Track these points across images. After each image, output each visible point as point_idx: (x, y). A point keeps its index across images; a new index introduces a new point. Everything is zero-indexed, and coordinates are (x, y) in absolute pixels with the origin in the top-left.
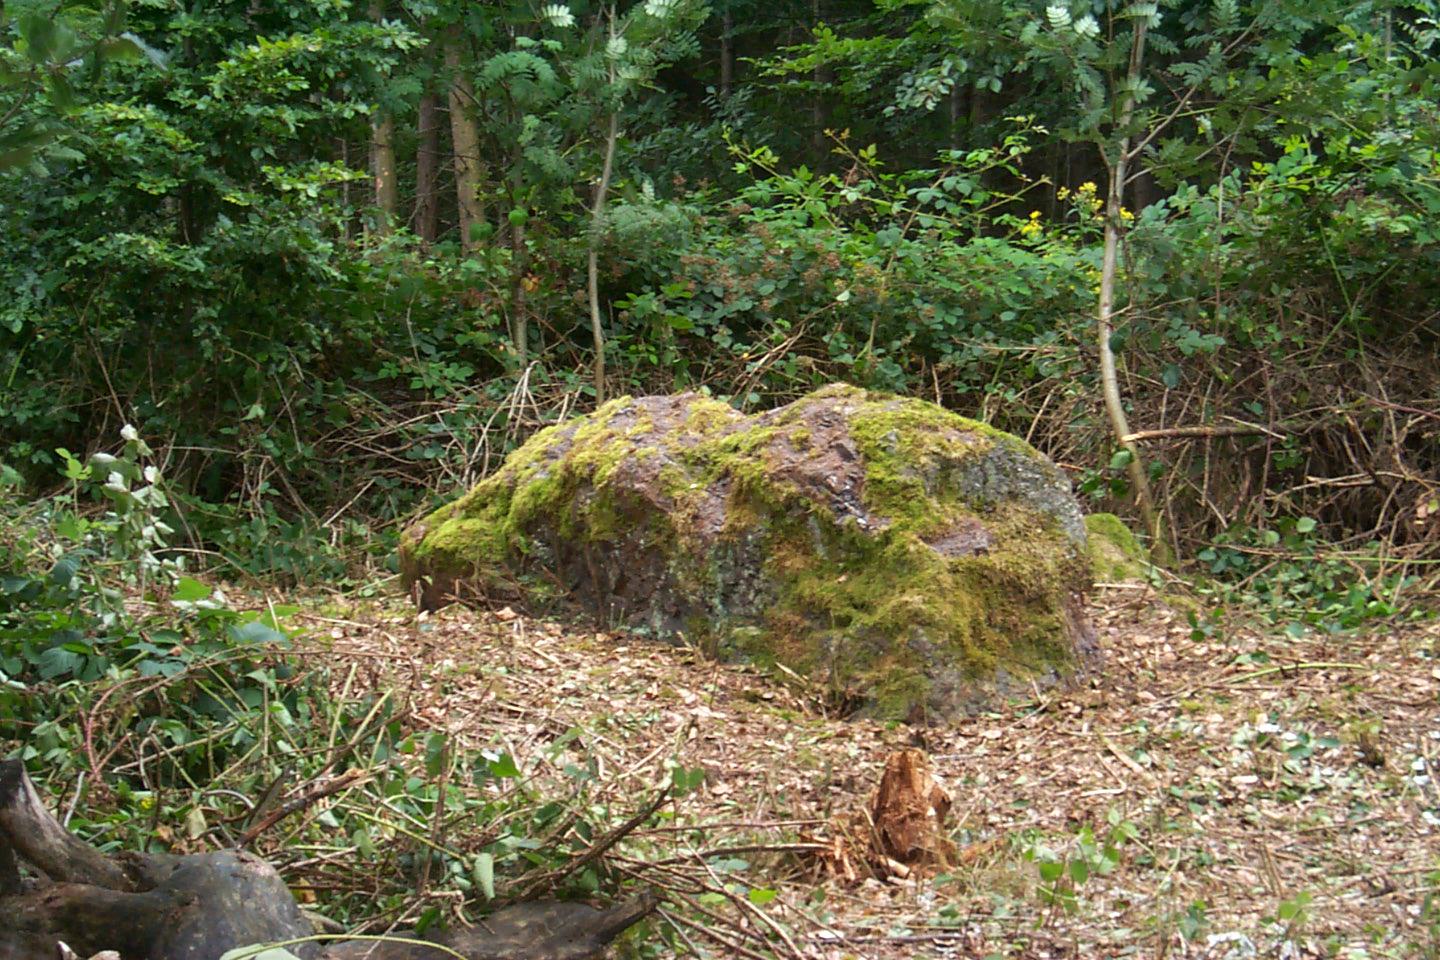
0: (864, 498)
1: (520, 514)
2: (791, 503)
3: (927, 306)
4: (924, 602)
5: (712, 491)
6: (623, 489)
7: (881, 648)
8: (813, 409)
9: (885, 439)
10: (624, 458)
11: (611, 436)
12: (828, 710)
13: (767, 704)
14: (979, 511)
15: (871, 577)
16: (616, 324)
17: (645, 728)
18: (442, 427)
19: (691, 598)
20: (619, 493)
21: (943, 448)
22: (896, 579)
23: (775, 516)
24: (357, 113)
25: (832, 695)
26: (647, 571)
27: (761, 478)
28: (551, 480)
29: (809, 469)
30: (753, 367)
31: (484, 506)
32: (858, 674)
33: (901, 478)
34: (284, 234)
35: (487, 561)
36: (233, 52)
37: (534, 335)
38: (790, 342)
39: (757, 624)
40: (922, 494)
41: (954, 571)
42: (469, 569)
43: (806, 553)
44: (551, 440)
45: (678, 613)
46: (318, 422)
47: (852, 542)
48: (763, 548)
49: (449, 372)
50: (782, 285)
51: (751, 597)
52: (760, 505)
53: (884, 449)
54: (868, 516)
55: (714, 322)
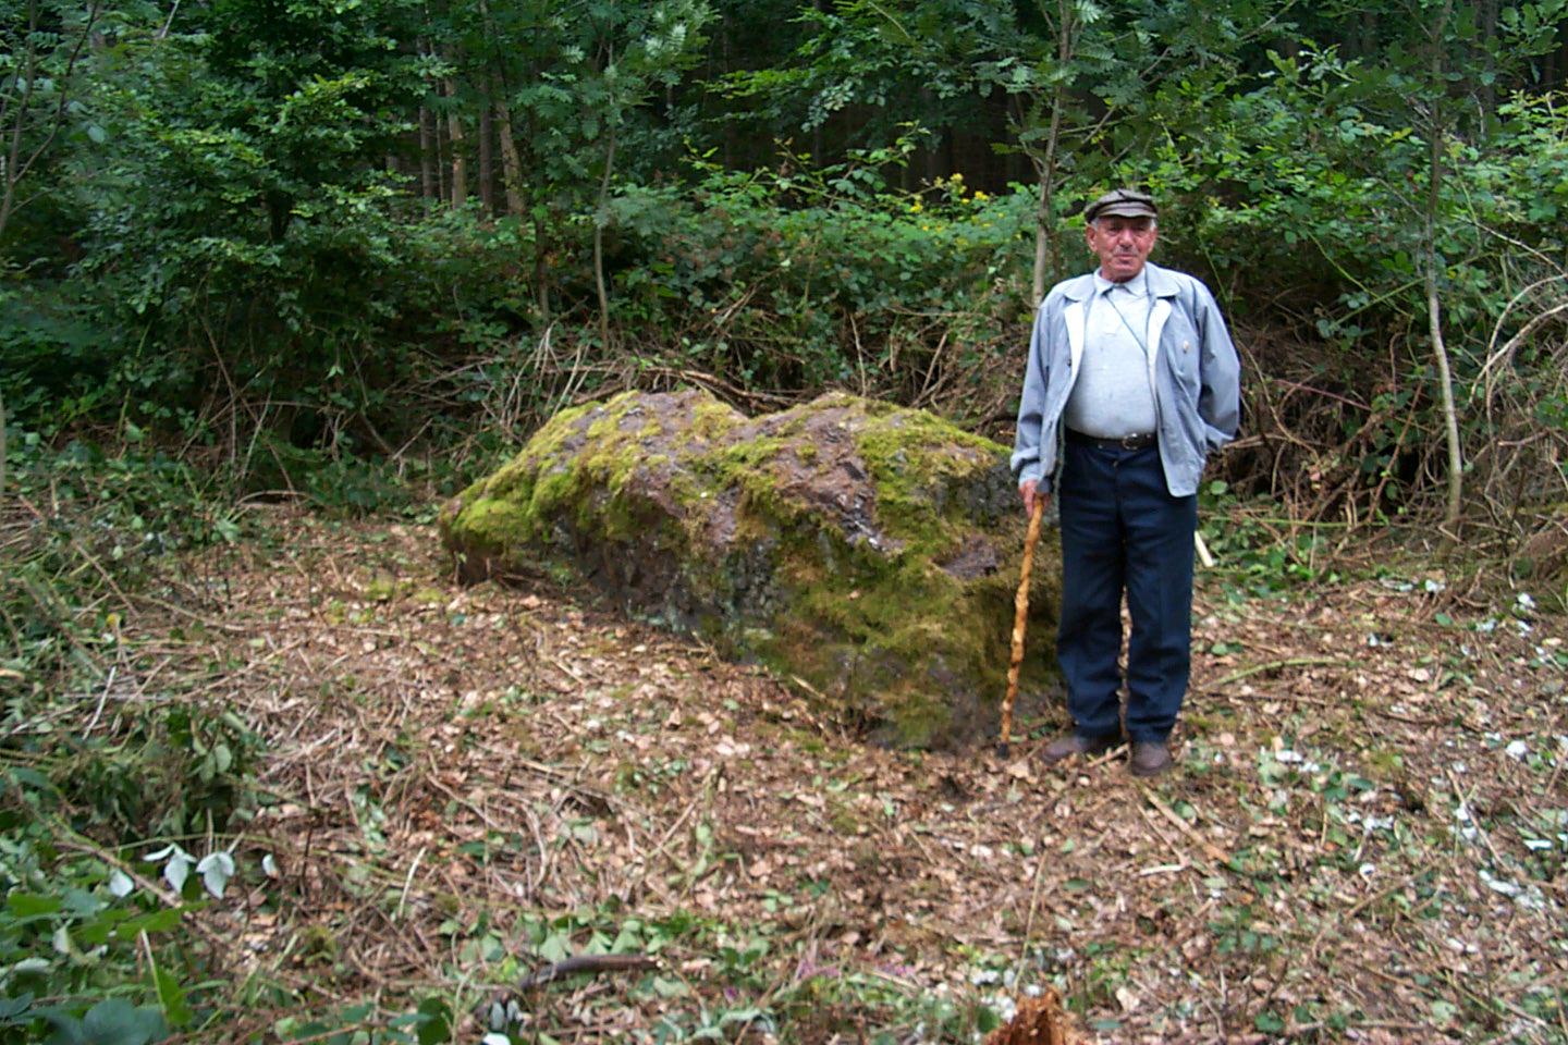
0: (876, 518)
1: (542, 504)
2: (802, 517)
3: (846, 270)
4: (944, 630)
5: (722, 499)
6: (636, 497)
7: (899, 671)
8: (817, 422)
9: (894, 459)
10: (637, 465)
11: (623, 439)
12: (846, 727)
13: (787, 725)
14: (984, 525)
15: (883, 595)
16: (621, 302)
17: (672, 779)
18: (484, 376)
20: (633, 499)
21: (951, 467)
22: (912, 603)
25: (850, 711)
26: (661, 568)
28: (568, 476)
29: (819, 485)
30: (720, 321)
31: (510, 489)
34: (347, 232)
35: (514, 542)
36: (300, 84)
37: (554, 298)
38: (746, 298)
40: (933, 516)
41: (969, 594)
42: (499, 548)
43: (815, 565)
44: (567, 431)
45: (692, 610)
47: (865, 561)
48: (773, 559)
49: (488, 331)
50: (739, 255)
51: (762, 601)
52: (770, 518)
53: (893, 470)
54: (879, 536)
55: (688, 286)
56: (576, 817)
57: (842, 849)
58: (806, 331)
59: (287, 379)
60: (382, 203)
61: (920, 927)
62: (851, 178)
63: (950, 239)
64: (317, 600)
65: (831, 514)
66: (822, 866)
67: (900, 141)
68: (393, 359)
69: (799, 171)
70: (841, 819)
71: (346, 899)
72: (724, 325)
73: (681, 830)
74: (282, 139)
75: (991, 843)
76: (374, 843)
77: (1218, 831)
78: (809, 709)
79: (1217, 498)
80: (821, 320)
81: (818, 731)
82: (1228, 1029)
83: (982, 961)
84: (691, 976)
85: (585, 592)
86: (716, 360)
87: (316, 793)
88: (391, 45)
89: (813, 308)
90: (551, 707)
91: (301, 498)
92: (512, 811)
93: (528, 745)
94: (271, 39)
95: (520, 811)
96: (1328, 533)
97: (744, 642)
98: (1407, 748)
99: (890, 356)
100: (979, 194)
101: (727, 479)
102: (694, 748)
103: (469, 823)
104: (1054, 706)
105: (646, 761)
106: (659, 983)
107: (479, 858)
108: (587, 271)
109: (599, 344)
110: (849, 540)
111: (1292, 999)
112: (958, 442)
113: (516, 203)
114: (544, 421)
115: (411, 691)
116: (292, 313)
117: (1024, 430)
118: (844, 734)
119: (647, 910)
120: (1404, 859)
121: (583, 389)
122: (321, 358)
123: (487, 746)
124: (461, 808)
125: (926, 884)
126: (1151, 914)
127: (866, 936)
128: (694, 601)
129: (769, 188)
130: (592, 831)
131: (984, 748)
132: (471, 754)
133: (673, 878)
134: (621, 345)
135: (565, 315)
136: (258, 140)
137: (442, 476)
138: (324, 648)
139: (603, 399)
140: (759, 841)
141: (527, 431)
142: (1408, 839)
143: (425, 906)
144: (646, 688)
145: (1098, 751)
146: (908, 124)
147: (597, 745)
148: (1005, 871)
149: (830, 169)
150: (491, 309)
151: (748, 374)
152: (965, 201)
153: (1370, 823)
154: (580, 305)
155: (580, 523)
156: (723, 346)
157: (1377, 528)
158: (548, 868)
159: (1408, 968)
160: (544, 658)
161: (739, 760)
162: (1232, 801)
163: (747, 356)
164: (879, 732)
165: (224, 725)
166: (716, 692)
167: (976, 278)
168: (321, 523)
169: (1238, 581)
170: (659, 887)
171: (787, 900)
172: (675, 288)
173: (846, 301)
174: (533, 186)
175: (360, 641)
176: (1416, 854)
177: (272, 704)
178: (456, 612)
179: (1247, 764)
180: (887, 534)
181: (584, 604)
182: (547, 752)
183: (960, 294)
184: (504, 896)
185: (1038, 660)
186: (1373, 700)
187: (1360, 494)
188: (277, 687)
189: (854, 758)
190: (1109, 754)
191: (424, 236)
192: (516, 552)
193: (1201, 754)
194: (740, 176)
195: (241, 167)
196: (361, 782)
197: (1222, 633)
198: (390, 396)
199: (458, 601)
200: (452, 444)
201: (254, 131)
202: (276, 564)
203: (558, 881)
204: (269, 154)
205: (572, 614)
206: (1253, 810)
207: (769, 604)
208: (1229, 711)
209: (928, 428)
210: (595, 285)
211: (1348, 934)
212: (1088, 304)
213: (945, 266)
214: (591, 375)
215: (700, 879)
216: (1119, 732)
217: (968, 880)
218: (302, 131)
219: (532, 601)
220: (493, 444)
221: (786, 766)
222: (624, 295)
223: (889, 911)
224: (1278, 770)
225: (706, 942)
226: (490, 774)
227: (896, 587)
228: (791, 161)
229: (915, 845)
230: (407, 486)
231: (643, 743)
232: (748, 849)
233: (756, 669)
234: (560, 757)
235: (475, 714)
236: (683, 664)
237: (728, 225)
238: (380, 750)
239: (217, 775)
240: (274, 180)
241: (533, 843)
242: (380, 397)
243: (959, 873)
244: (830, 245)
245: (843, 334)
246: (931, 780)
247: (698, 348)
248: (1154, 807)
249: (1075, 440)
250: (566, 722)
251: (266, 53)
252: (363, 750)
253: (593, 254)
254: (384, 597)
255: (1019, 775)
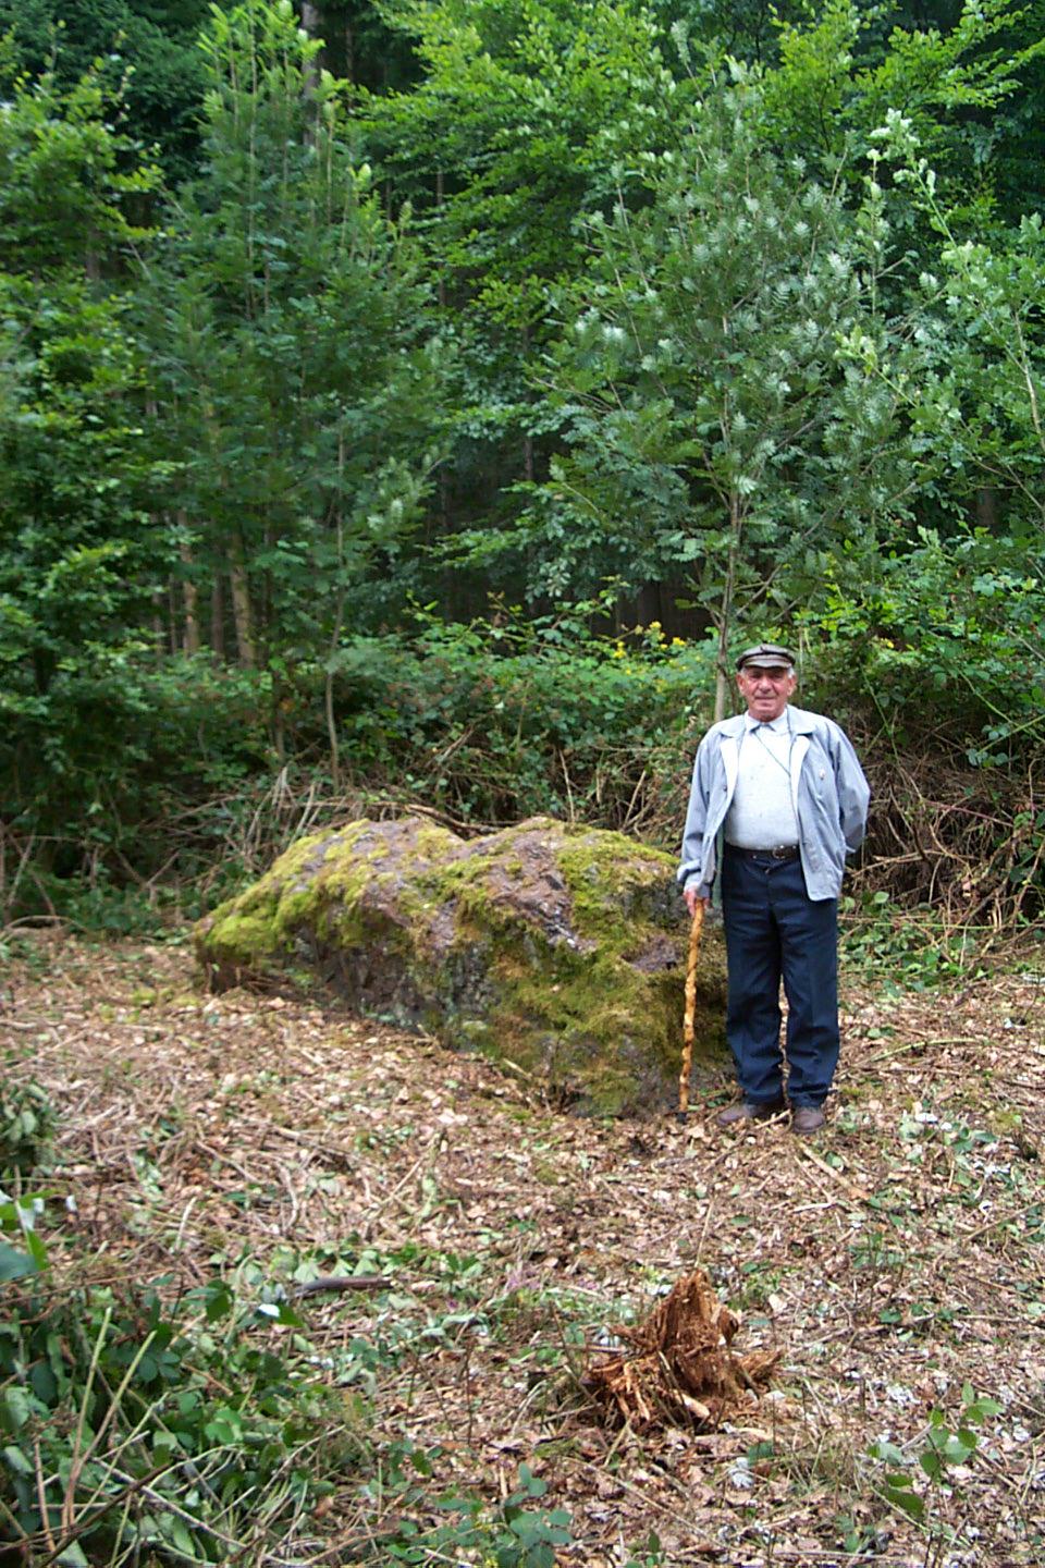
1: (286, 919)
2: (510, 924)
3: (555, 711)
8: (522, 842)
9: (587, 872)
10: (368, 882)
15: (580, 988)
16: (352, 742)
18: (226, 812)
19: (428, 997)
20: (365, 912)
23: (496, 934)
24: (884, 125)
25: (554, 1088)
27: (483, 904)
29: (524, 896)
30: (440, 759)
31: (256, 907)
32: (574, 1072)
33: (603, 906)
35: (260, 953)
36: (64, 554)
38: (464, 738)
39: (483, 1019)
40: (621, 920)
42: (247, 959)
43: (523, 964)
44: (307, 855)
45: (417, 1006)
46: (139, 811)
47: (564, 959)
48: (486, 961)
49: (230, 771)
50: (456, 699)
51: (477, 997)
52: (483, 925)
56: (321, 1172)
57: (545, 1196)
58: (518, 767)
59: (49, 818)
60: (135, 657)
61: (609, 1253)
62: (559, 628)
63: (650, 681)
64: (89, 1005)
65: (535, 920)
66: (527, 1209)
67: (603, 594)
68: (145, 797)
69: (511, 622)
70: (544, 1172)
71: (131, 1237)
72: (444, 763)
73: (409, 1182)
74: (49, 602)
75: (669, 1189)
76: (154, 1195)
77: (862, 1177)
78: (519, 1087)
79: (879, 906)
80: (534, 757)
81: (527, 1105)
82: (857, 1323)
83: (660, 1278)
84: (418, 1293)
85: (324, 995)
86: (438, 796)
87: (102, 1156)
88: (144, 518)
89: (525, 746)
90: (297, 1085)
91: (62, 923)
92: (267, 1167)
93: (280, 1116)
94: (37, 515)
95: (274, 1168)
96: (978, 935)
97: (462, 1033)
98: (1027, 1108)
99: (597, 789)
100: (676, 640)
101: (446, 892)
102: (419, 1117)
103: (232, 1178)
104: (728, 1081)
105: (379, 1128)
106: (392, 1298)
107: (241, 1204)
108: (319, 717)
109: (329, 781)
110: (550, 941)
111: (910, 1298)
112: (643, 857)
113: (247, 650)
114: (281, 852)
115: (178, 1075)
116: (57, 757)
117: (689, 846)
118: (548, 1108)
119: (381, 1244)
120: (1018, 1196)
121: (317, 823)
122: (84, 796)
123: (244, 1116)
124: (226, 1166)
125: (615, 1221)
126: (801, 1241)
127: (563, 1262)
128: (419, 998)
129: (484, 638)
130: (334, 1184)
131: (667, 1116)
132: (232, 1122)
133: (402, 1221)
134: (351, 783)
135: (299, 755)
136: (26, 604)
137: (189, 903)
138: (99, 1042)
139: (337, 829)
140: (475, 1190)
141: (266, 862)
142: (1023, 1181)
143: (198, 1242)
144: (378, 1070)
145: (764, 1117)
146: (611, 578)
147: (337, 1116)
148: (681, 1211)
149: (537, 622)
150: (232, 752)
151: (467, 807)
152: (664, 646)
153: (990, 1168)
154: (312, 747)
155: (319, 934)
156: (443, 782)
157: (1019, 930)
158: (299, 1212)
159: (1012, 1279)
160: (291, 1047)
161: (458, 1127)
162: (875, 1153)
163: (465, 790)
164: (579, 1105)
165: (29, 1095)
166: (438, 1074)
167: (675, 716)
168: (82, 945)
169: (898, 979)
170: (393, 1229)
171: (499, 1236)
172: (400, 729)
173: (555, 739)
174: (269, 640)
175: (130, 1037)
176: (1027, 1193)
177: (61, 1085)
178: (212, 1013)
179: (891, 1124)
180: (582, 935)
181: (323, 1004)
182: (296, 1121)
183: (659, 731)
184: (263, 1234)
185: (707, 1041)
186: (1001, 1071)
187: (1004, 900)
188: (65, 1071)
189: (556, 1125)
190: (774, 1118)
191: (167, 684)
192: (263, 962)
193: (849, 1117)
194: (457, 627)
195: (12, 628)
196: (141, 1146)
197: (877, 1020)
198: (139, 832)
199: (212, 1004)
200: (198, 874)
201: (23, 596)
202: (45, 980)
203: (307, 1223)
204: (37, 616)
205: (312, 1014)
206: (893, 1160)
207: (483, 1000)
208: (879, 1082)
209: (617, 846)
210: (327, 729)
211: (966, 1255)
212: (741, 739)
213: (645, 707)
214: (324, 810)
215: (425, 1220)
216: (782, 1100)
217: (650, 1217)
218: (66, 596)
219: (278, 1002)
220: (236, 873)
221: (500, 1131)
222: (354, 737)
223: (583, 1242)
224: (916, 1128)
225: (431, 1269)
226: (249, 1139)
227: (590, 981)
228: (503, 613)
229: (606, 1191)
230: (158, 911)
231: (376, 1114)
232: (466, 1197)
233: (473, 1056)
234: (306, 1125)
235: (234, 1091)
236: (409, 1053)
237: (446, 672)
238: (154, 1121)
239: (24, 1136)
240: (40, 640)
241: (285, 1193)
242: (132, 832)
243: (642, 1212)
244: (540, 690)
245: (553, 770)
246: (621, 1141)
247: (421, 784)
248: (808, 1159)
249: (733, 855)
250: (311, 1097)
251: (34, 528)
252: (140, 1121)
253: (324, 701)
254: (147, 1002)
255: (696, 1136)
